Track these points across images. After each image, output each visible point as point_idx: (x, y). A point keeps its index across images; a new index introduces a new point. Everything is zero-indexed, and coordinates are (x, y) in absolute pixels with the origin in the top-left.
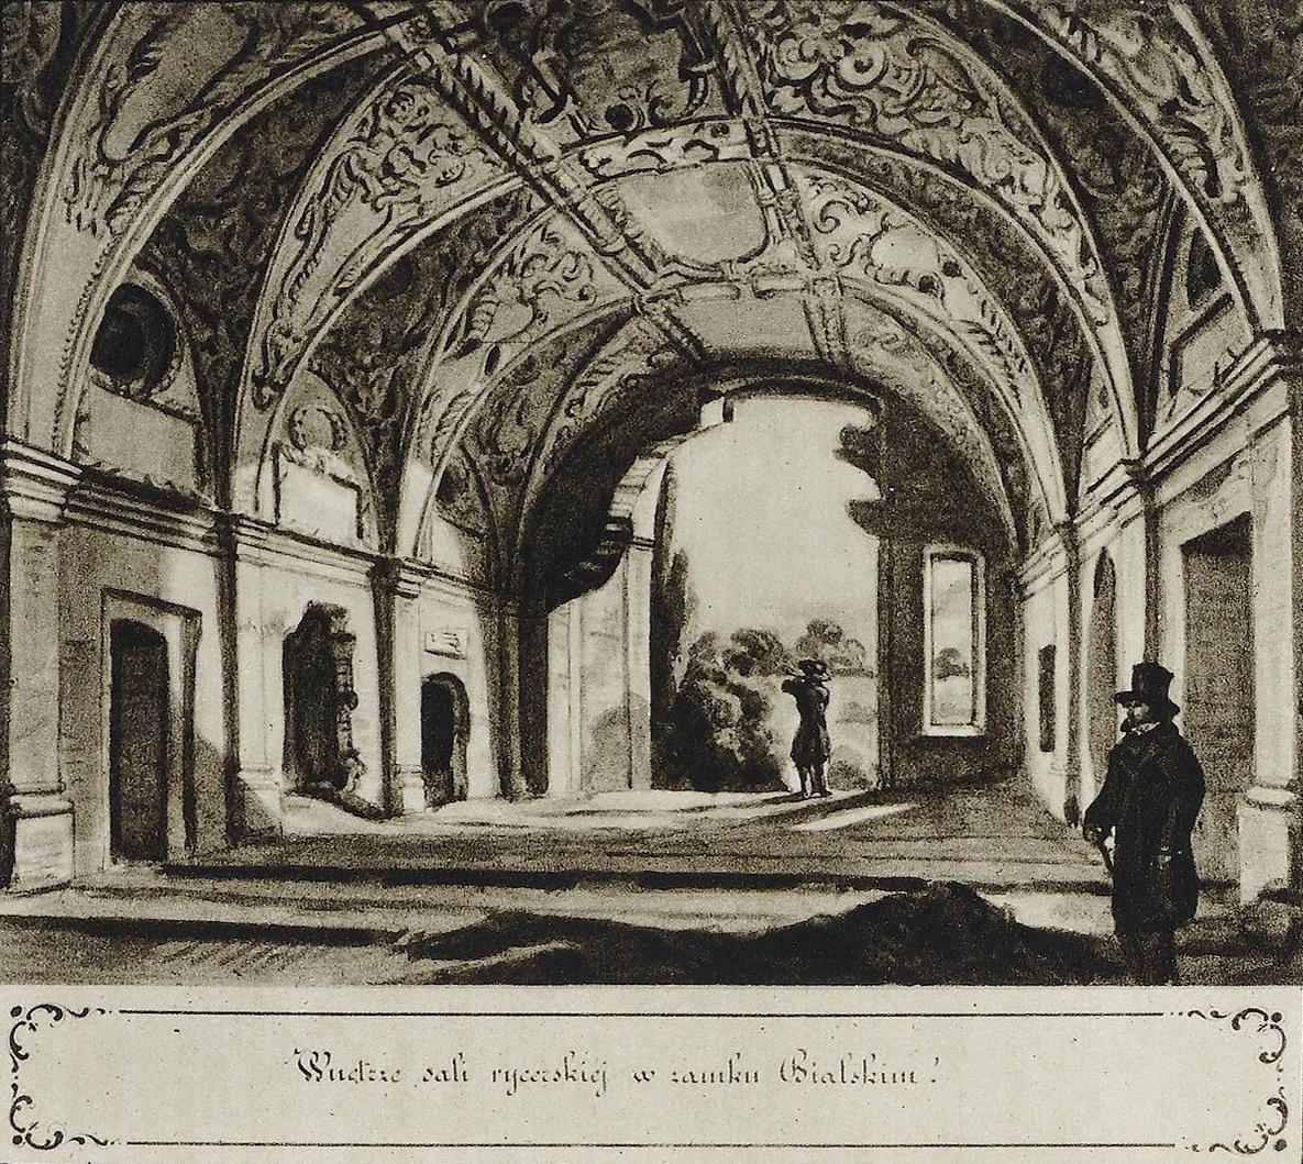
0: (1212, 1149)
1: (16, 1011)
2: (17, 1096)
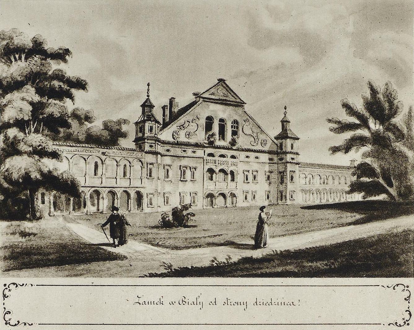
0: (389, 325)
1: (5, 285)
2: (408, 300)
